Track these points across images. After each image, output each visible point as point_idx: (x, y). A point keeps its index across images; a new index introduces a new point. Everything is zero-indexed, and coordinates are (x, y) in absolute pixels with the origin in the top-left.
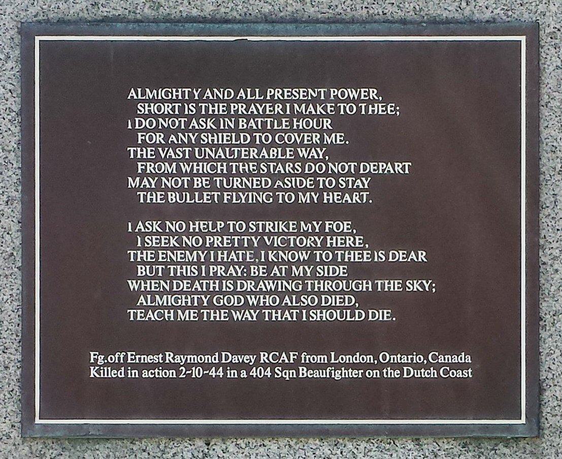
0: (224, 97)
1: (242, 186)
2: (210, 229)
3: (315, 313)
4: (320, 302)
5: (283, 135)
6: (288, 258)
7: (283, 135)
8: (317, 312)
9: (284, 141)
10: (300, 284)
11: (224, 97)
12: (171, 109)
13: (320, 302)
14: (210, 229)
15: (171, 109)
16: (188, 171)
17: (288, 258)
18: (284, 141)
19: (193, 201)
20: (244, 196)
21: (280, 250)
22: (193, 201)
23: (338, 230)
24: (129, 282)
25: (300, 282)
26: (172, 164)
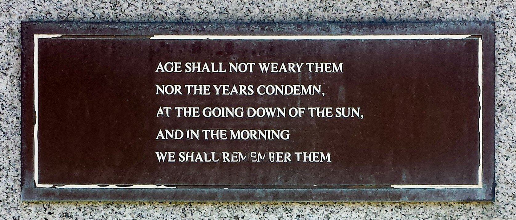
0: (284, 92)
1: (258, 138)
2: (213, 159)
3: (341, 110)
4: (351, 115)
5: (265, 86)
6: (238, 69)
7: (265, 86)
8: (342, 109)
9: (265, 93)
10: (242, 111)
11: (284, 92)
12: (228, 157)
13: (351, 115)
14: (213, 159)
15: (228, 157)
16: (273, 115)
17: (238, 69)
18: (265, 93)
19: (210, 161)
20: (300, 66)
21: (273, 129)
22: (210, 161)
23: (261, 115)
24: (157, 153)
25: (242, 109)
26: (339, 64)
